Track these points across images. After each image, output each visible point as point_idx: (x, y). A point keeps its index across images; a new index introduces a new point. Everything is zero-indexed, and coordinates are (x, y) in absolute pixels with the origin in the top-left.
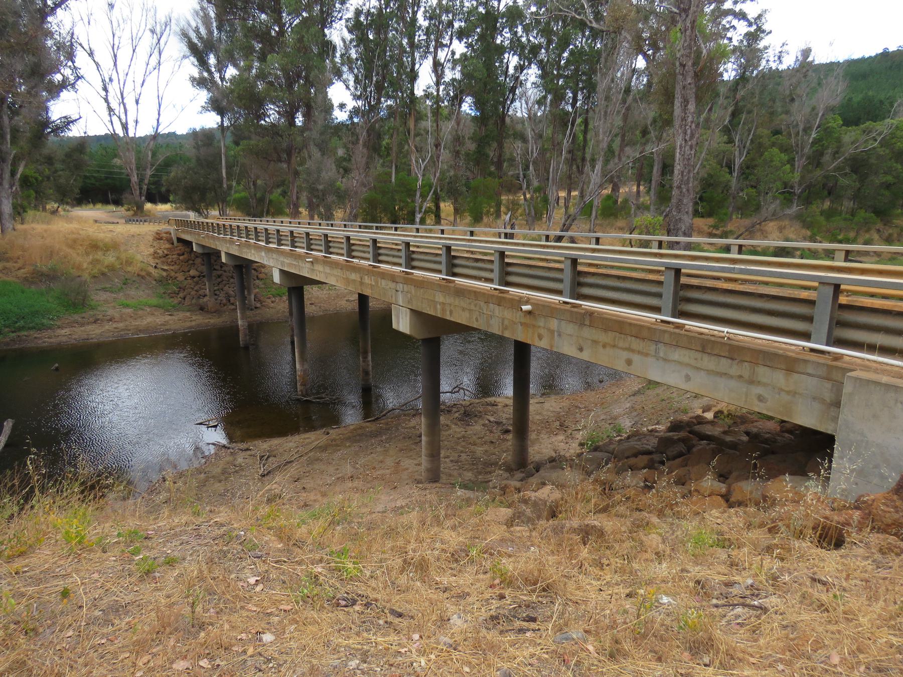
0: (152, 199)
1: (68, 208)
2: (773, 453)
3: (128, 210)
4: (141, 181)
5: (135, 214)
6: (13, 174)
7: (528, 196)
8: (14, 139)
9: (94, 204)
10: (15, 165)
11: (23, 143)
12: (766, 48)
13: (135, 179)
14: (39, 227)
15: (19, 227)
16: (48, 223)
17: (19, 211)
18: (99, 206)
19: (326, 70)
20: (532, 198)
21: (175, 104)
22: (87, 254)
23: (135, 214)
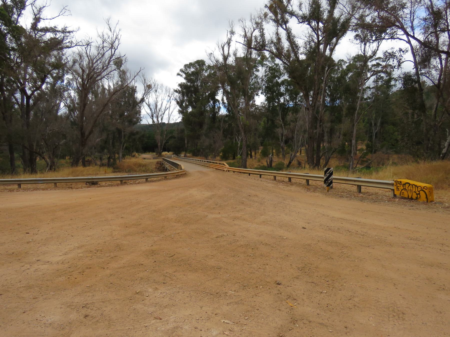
0: (165, 150)
1: (140, 154)
2: (230, 43)
3: (156, 155)
4: (161, 145)
5: (159, 156)
6: (123, 146)
7: (18, 95)
8: (124, 137)
9: (149, 152)
10: (124, 144)
11: (126, 138)
12: (184, 174)
13: (159, 144)
14: (128, 160)
15: (123, 160)
16: (130, 159)
17: (124, 156)
18: (151, 153)
19: (55, 38)
20: (12, 93)
21: (173, 115)
22: (138, 167)
23: (159, 156)
